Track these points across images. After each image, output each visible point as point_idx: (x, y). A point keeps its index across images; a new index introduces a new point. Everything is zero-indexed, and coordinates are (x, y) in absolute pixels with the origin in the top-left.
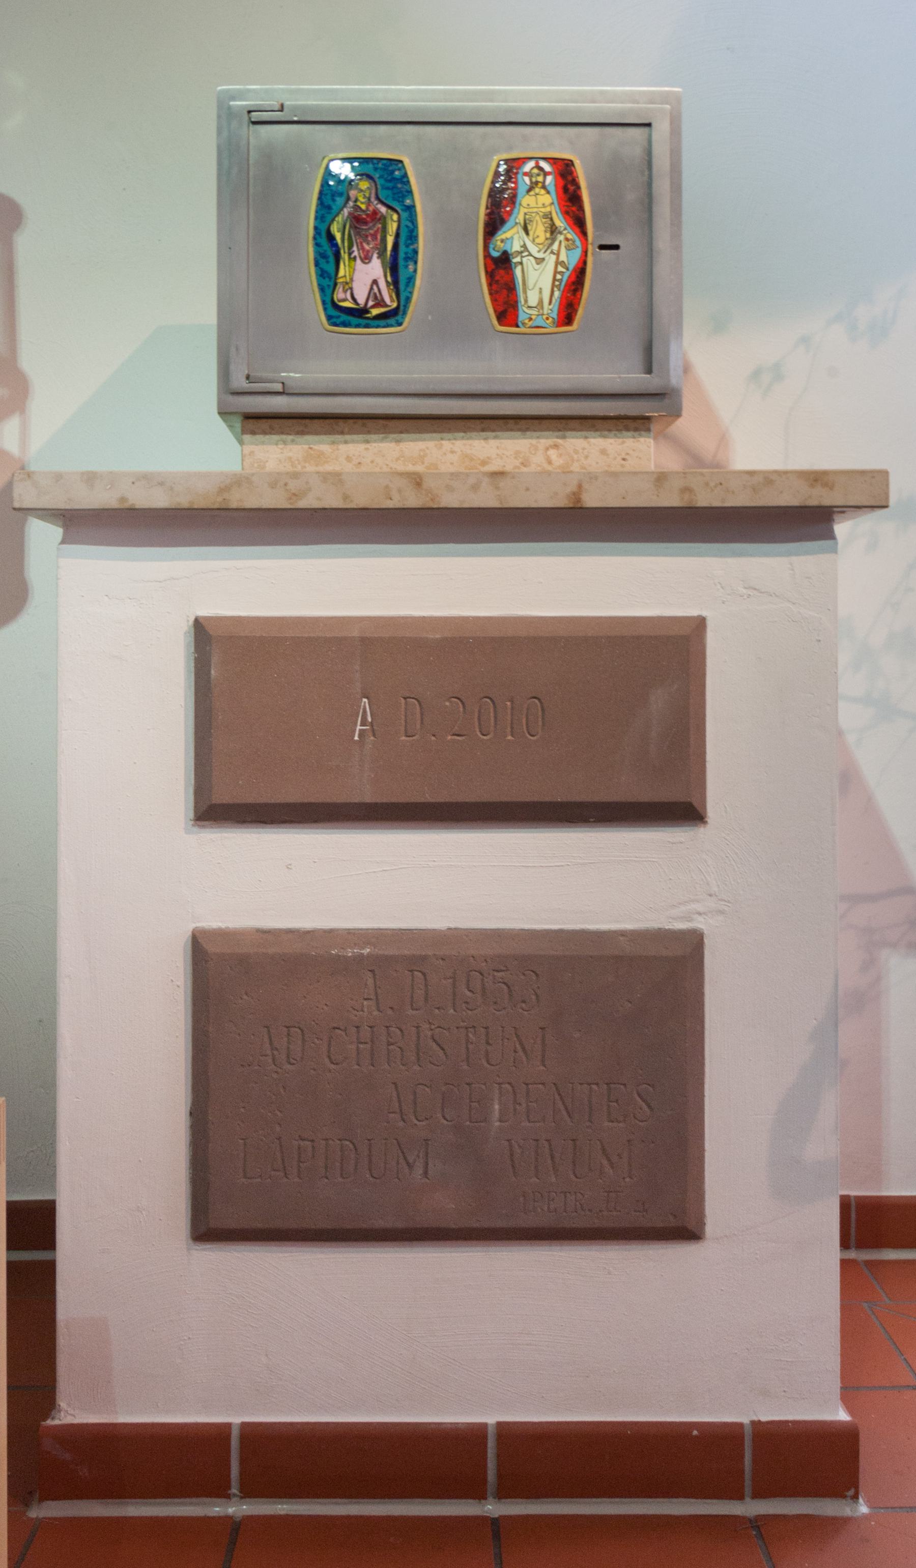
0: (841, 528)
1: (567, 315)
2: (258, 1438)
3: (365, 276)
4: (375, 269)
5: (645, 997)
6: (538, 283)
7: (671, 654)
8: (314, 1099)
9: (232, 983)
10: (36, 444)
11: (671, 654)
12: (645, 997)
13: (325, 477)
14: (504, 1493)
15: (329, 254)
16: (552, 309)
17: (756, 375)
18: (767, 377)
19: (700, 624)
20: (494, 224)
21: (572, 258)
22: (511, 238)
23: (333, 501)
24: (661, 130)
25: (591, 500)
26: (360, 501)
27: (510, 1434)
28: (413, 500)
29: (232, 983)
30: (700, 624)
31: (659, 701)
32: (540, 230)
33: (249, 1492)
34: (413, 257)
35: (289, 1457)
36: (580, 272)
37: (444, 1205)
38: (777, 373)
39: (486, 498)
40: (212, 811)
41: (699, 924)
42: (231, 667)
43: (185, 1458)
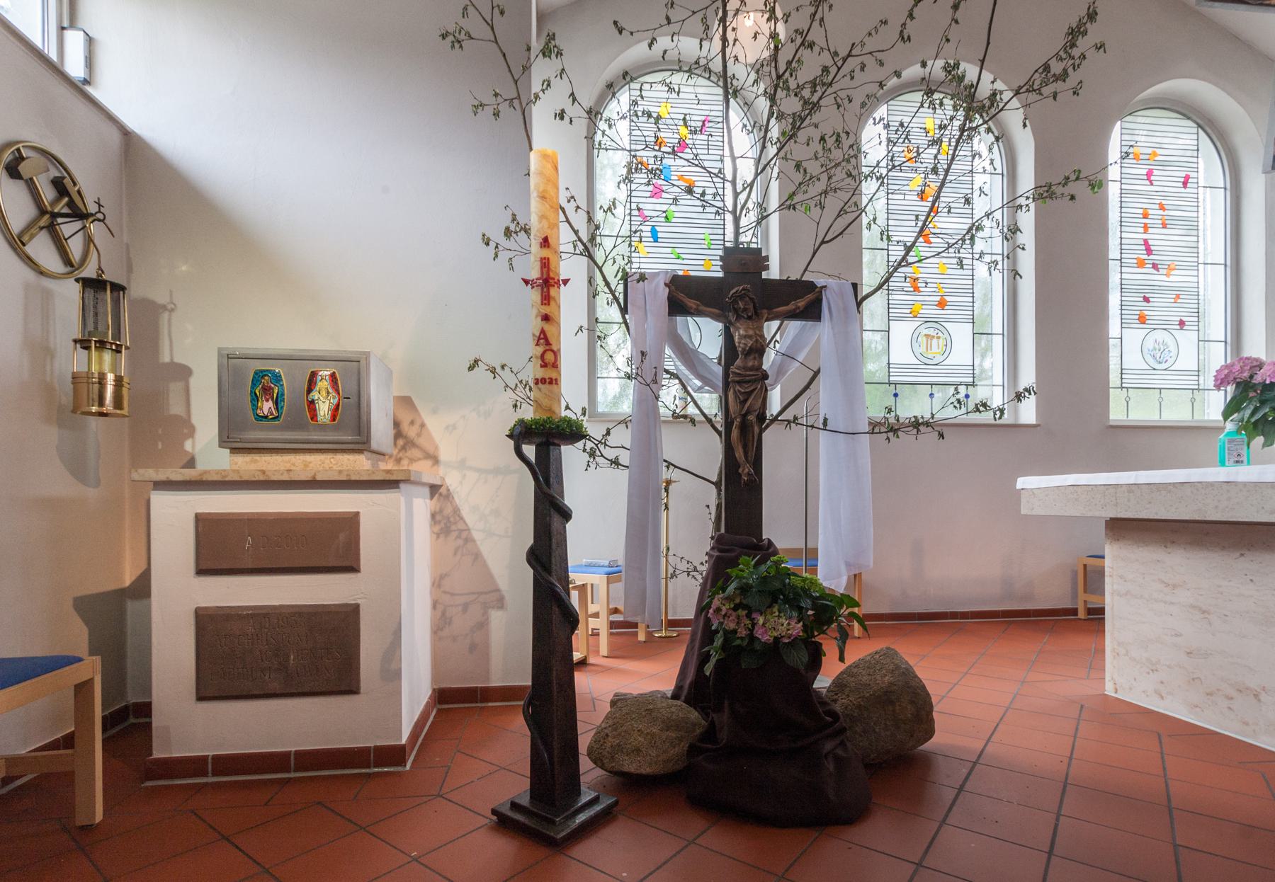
0: (402, 485)
1: (334, 418)
2: (378, 749)
3: (267, 406)
4: (270, 404)
5: (339, 627)
6: (324, 409)
7: (351, 522)
8: (239, 657)
9: (210, 625)
10: (199, 447)
11: (351, 522)
12: (339, 627)
13: (234, 471)
14: (296, 770)
15: (255, 398)
16: (328, 417)
17: (447, 427)
18: (451, 428)
19: (357, 514)
20: (310, 390)
21: (335, 401)
22: (315, 395)
23: (237, 478)
24: (363, 362)
25: (318, 478)
26: (245, 478)
27: (298, 754)
28: (262, 478)
29: (210, 625)
30: (357, 514)
31: (342, 537)
32: (324, 393)
33: (214, 775)
34: (283, 400)
35: (226, 764)
36: (338, 405)
37: (275, 686)
38: (454, 427)
39: (285, 477)
40: (201, 572)
41: (359, 601)
42: (206, 526)
43: (196, 766)
